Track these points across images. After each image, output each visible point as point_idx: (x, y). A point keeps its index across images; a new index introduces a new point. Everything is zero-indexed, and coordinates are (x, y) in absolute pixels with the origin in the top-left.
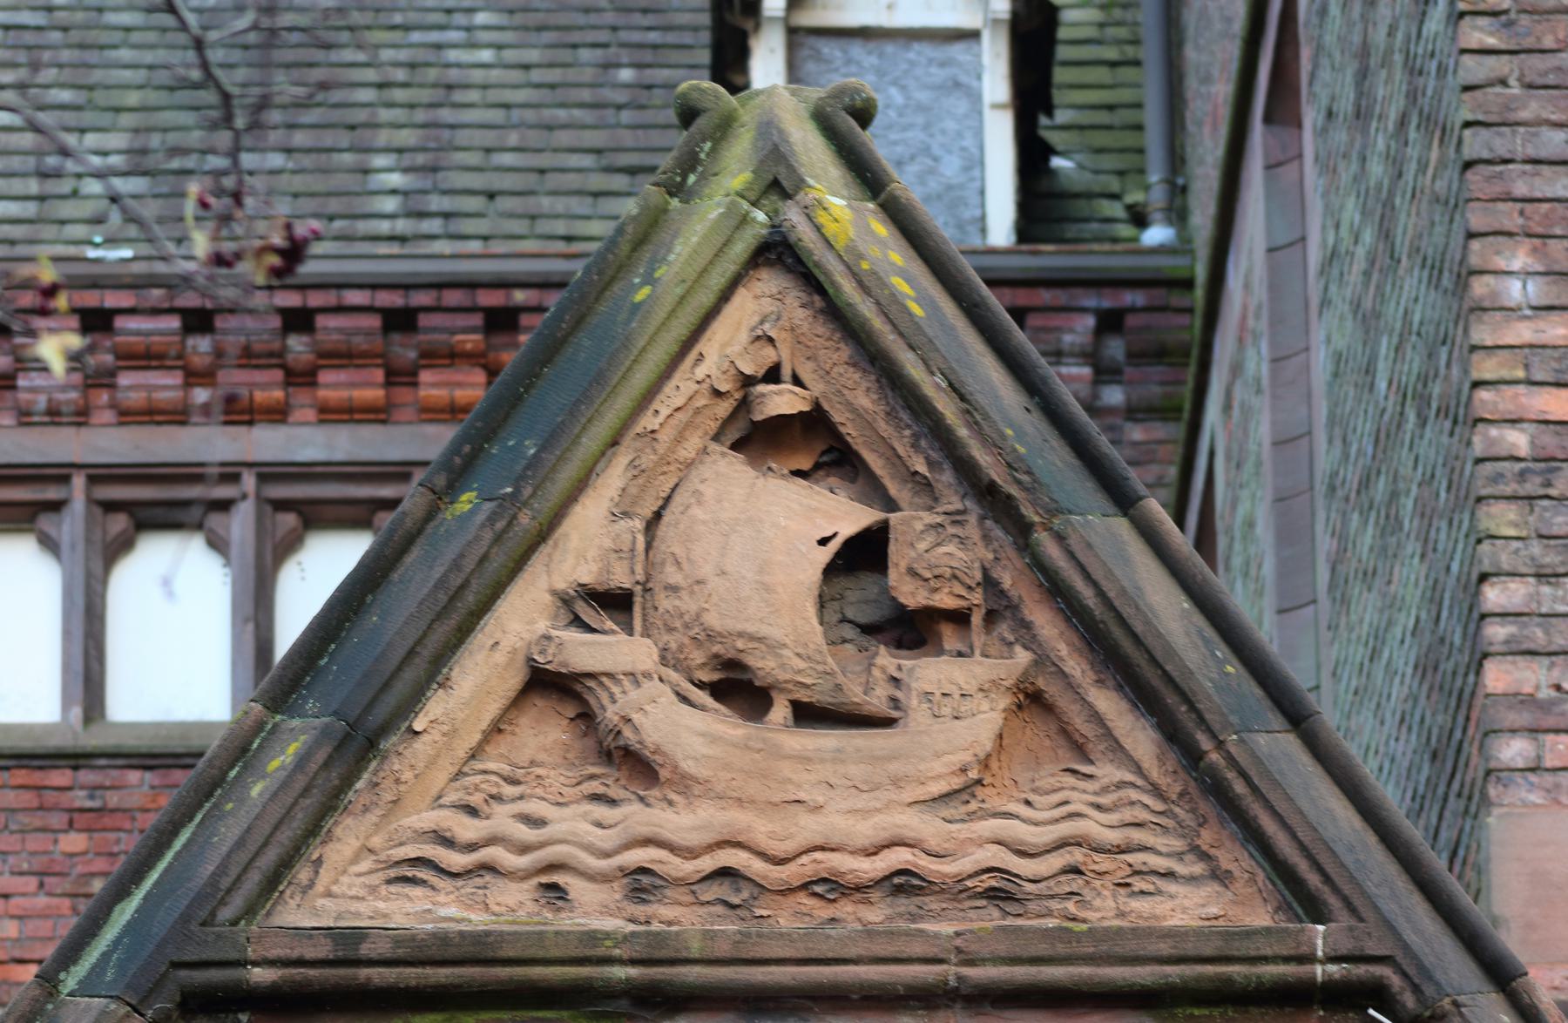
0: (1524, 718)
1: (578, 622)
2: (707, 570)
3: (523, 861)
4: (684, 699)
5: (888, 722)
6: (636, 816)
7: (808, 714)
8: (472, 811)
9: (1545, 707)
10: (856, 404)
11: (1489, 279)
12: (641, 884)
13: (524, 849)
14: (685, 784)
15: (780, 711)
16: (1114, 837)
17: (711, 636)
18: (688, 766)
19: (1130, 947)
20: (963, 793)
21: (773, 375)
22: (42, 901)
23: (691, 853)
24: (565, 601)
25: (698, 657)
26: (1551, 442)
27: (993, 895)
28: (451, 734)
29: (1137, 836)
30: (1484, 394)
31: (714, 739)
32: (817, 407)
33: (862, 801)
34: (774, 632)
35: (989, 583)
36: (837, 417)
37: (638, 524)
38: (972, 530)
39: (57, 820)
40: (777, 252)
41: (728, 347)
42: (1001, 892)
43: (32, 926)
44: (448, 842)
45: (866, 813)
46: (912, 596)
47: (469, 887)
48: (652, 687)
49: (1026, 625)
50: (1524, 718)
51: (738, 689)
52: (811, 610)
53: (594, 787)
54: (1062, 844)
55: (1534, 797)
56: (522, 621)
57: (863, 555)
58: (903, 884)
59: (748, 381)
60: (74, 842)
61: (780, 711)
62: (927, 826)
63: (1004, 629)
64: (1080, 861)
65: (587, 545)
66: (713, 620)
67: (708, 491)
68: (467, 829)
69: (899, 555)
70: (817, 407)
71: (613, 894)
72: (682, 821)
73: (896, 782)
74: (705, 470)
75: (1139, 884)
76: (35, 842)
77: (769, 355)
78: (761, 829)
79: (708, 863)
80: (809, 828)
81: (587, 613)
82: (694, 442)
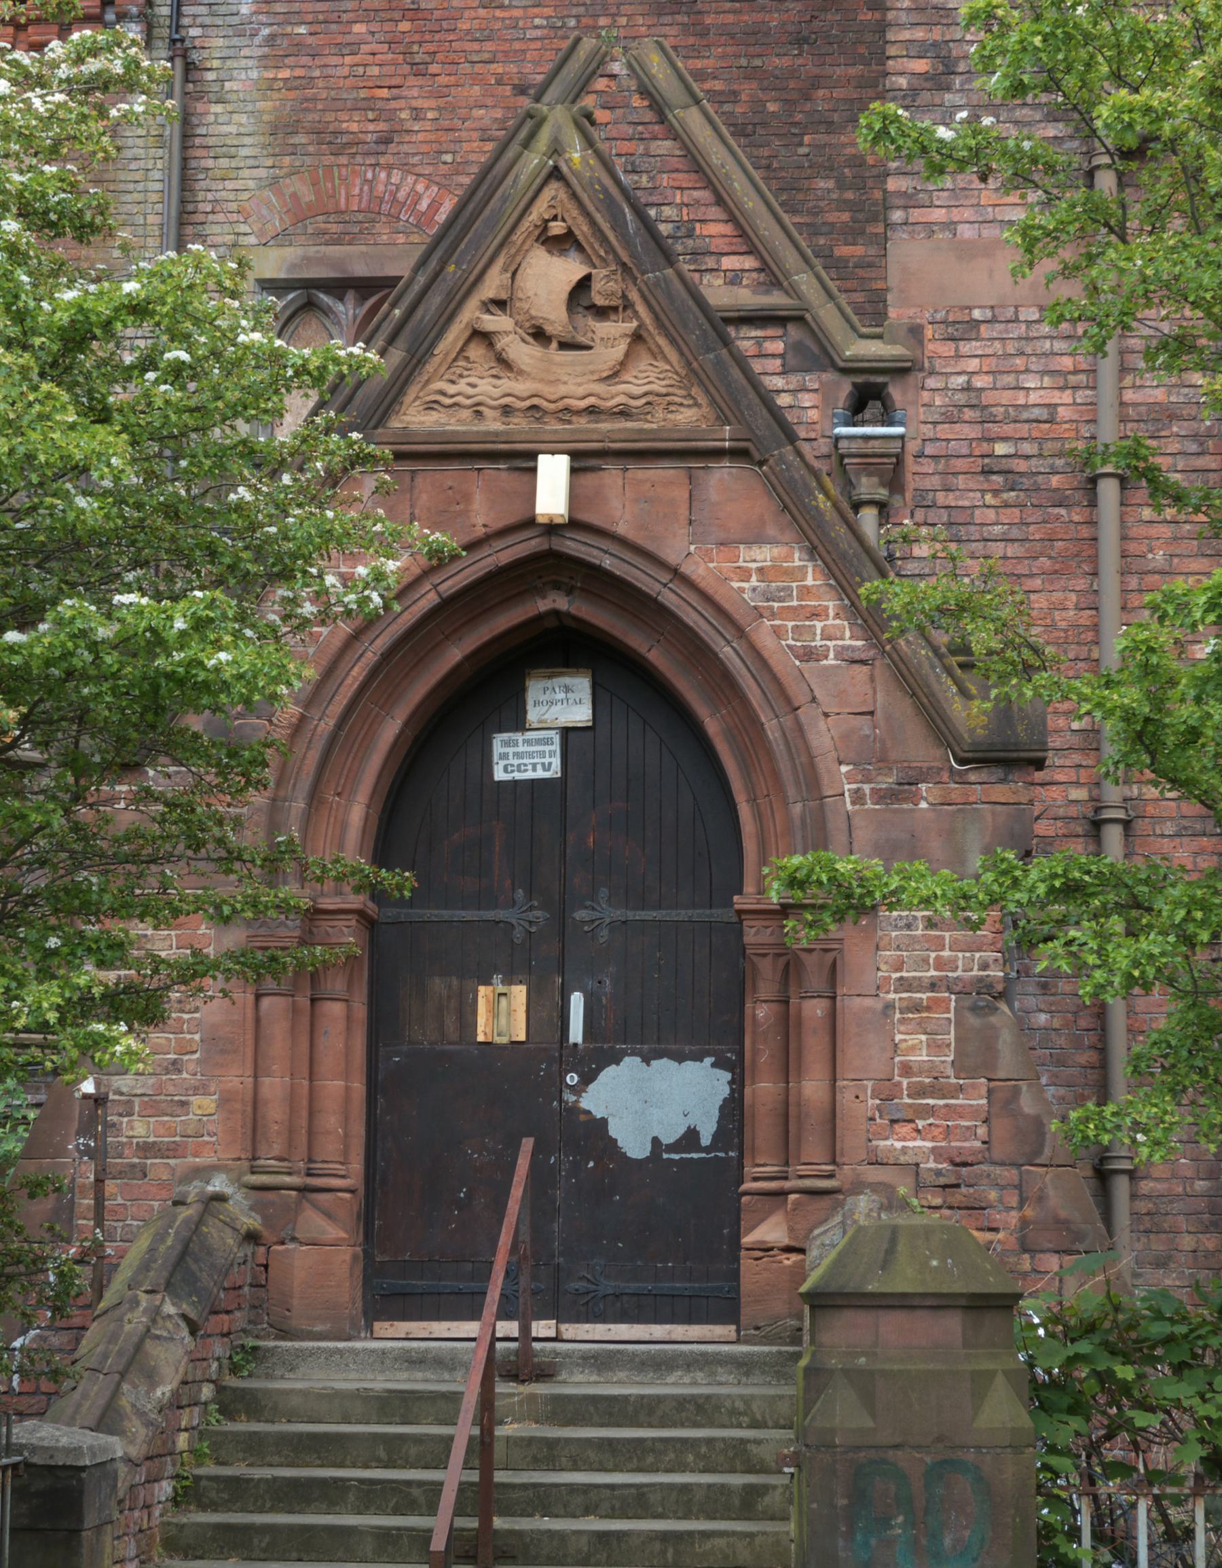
0: (901, 202)
1: (489, 311)
2: (530, 293)
3: (469, 402)
4: (523, 340)
5: (589, 348)
6: (507, 384)
7: (564, 346)
8: (453, 382)
9: (910, 197)
10: (582, 230)
11: (894, 12)
12: (507, 410)
13: (469, 397)
14: (521, 372)
15: (554, 345)
16: (664, 390)
17: (532, 318)
18: (523, 367)
19: (665, 435)
20: (614, 376)
21: (555, 218)
22: (390, 56)
23: (523, 399)
24: (484, 304)
25: (527, 325)
26: (916, 83)
27: (622, 413)
28: (447, 354)
29: (671, 390)
30: (890, 62)
31: (532, 357)
32: (569, 229)
33: (579, 380)
34: (552, 317)
35: (624, 296)
36: (577, 232)
37: (509, 275)
38: (619, 277)
39: (397, 15)
40: (556, 174)
41: (540, 210)
42: (624, 413)
43: (386, 70)
44: (443, 393)
45: (580, 385)
46: (600, 301)
47: (451, 411)
48: (512, 336)
49: (636, 312)
50: (901, 202)
51: (540, 335)
52: (564, 308)
53: (494, 372)
54: (646, 394)
55: (905, 236)
56: (470, 313)
57: (584, 284)
58: (592, 411)
59: (547, 221)
60: (405, 26)
61: (554, 345)
62: (600, 388)
63: (629, 312)
64: (651, 400)
65: (492, 286)
66: (533, 312)
67: (533, 261)
68: (452, 389)
69: (597, 285)
70: (569, 229)
71: (497, 413)
72: (522, 387)
73: (592, 373)
74: (531, 254)
75: (672, 408)
76: (388, 26)
77: (554, 212)
78: (547, 390)
79: (528, 403)
80: (562, 390)
81: (493, 308)
82: (529, 242)
